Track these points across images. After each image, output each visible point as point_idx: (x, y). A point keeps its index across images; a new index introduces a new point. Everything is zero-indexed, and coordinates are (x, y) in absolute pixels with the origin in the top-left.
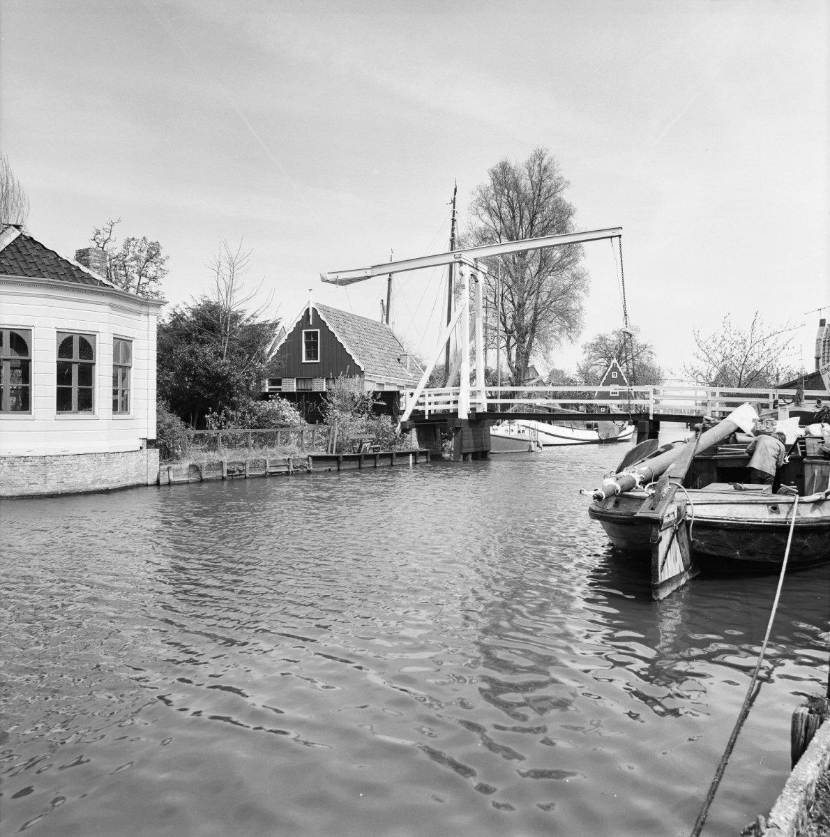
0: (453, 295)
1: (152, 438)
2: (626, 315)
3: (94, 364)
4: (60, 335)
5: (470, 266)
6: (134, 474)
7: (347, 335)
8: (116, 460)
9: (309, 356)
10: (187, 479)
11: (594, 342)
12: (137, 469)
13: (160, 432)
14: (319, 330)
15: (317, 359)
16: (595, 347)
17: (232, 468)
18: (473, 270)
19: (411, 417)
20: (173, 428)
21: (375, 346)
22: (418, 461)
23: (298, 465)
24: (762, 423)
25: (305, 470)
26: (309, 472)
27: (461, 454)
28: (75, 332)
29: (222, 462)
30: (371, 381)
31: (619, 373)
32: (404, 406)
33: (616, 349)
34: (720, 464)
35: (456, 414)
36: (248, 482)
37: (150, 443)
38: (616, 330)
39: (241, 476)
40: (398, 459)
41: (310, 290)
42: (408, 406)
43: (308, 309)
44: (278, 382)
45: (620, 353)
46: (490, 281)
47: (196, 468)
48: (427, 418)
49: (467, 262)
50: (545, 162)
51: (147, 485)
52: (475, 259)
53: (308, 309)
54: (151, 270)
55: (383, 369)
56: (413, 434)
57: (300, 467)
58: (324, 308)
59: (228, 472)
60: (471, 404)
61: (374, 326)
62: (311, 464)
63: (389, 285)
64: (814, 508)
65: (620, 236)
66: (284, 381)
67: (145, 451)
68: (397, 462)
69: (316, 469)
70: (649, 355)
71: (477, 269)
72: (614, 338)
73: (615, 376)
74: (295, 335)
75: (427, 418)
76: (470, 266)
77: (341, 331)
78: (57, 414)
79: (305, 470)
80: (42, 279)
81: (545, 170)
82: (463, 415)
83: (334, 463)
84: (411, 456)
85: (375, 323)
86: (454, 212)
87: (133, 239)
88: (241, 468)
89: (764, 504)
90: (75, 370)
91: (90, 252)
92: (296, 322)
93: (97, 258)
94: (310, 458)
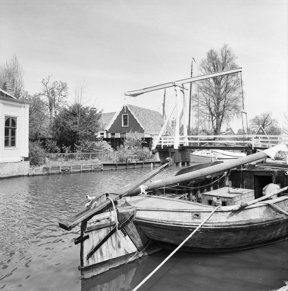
0: (191, 100)
1: (26, 157)
2: (243, 105)
3: (16, 128)
4: (6, 117)
5: (180, 87)
6: (17, 171)
7: (139, 116)
8: (6, 165)
9: (124, 125)
10: (42, 173)
11: (254, 118)
12: (19, 169)
13: (31, 154)
14: (128, 114)
16: (254, 120)
17: (64, 169)
18: (181, 89)
19: (156, 148)
20: (38, 153)
21: (151, 120)
22: (155, 166)
23: (96, 167)
24: (279, 154)
25: (100, 169)
26: (102, 170)
27: (175, 163)
28: (11, 116)
29: (59, 166)
30: (147, 134)
31: (263, 130)
32: (154, 143)
33: (262, 121)
34: (255, 174)
35: (173, 146)
36: (72, 174)
37: (26, 159)
38: (262, 114)
39: (69, 172)
40: (136, 166)
41: (125, 99)
42: (155, 144)
44: (113, 134)
45: (264, 122)
46: (204, 95)
47: (46, 169)
49: (177, 85)
50: (227, 49)
51: (24, 176)
52: (182, 84)
54: (63, 93)
55: (154, 129)
56: (157, 155)
57: (97, 168)
58: (130, 106)
59: (62, 170)
60: (180, 143)
61: (153, 113)
62: (103, 167)
63: (164, 97)
64: (231, 215)
66: (116, 134)
67: (23, 162)
68: (145, 166)
69: (104, 169)
70: (276, 123)
71: (183, 88)
72: (262, 117)
73: (261, 131)
74: (119, 117)
76: (180, 87)
77: (137, 114)
78: (5, 147)
79: (100, 169)
80: (2, 96)
81: (228, 51)
82: (176, 147)
83: (114, 167)
84: (152, 164)
85: (154, 112)
86: (192, 69)
87: (57, 82)
88: (68, 169)
89: (189, 212)
90: (10, 130)
91: (7, 83)
92: (120, 111)
93: (10, 86)
94: (102, 165)
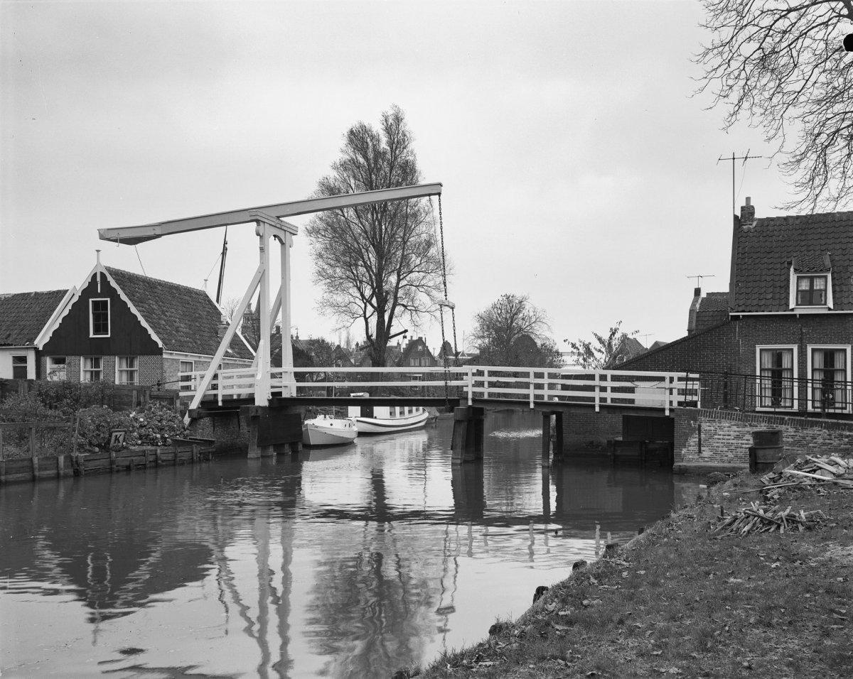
15: (107, 334)
19: (202, 403)
35: (251, 399)
43: (95, 274)
48: (220, 404)
53: (95, 274)
60: (272, 387)
65: (439, 194)
75: (220, 404)
82: (262, 400)
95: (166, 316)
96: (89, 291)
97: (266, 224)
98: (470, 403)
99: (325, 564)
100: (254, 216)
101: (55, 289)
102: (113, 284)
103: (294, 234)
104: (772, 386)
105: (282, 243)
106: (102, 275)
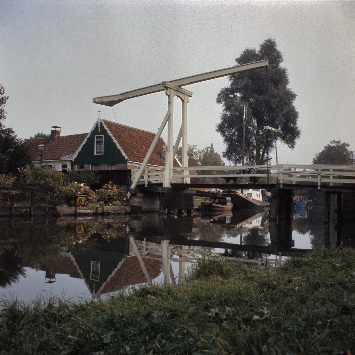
43: (98, 123)
53: (98, 123)
95: (133, 144)
96: (95, 131)
97: (171, 89)
98: (281, 186)
99: (154, 284)
100: (164, 87)
101: (84, 133)
102: (106, 128)
103: (190, 96)
104: (266, 253)
105: (183, 101)
106: (101, 124)
